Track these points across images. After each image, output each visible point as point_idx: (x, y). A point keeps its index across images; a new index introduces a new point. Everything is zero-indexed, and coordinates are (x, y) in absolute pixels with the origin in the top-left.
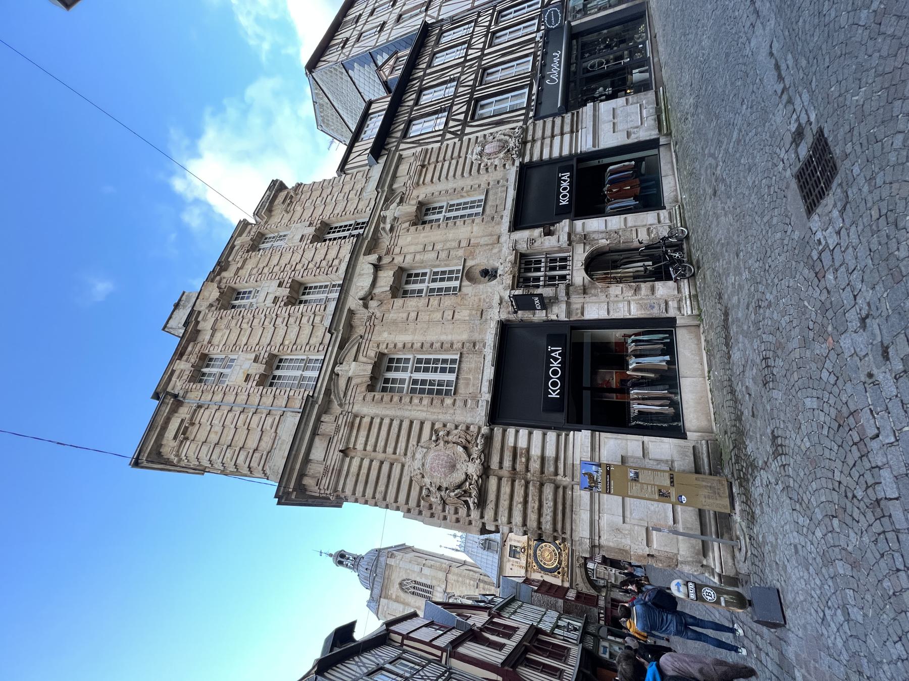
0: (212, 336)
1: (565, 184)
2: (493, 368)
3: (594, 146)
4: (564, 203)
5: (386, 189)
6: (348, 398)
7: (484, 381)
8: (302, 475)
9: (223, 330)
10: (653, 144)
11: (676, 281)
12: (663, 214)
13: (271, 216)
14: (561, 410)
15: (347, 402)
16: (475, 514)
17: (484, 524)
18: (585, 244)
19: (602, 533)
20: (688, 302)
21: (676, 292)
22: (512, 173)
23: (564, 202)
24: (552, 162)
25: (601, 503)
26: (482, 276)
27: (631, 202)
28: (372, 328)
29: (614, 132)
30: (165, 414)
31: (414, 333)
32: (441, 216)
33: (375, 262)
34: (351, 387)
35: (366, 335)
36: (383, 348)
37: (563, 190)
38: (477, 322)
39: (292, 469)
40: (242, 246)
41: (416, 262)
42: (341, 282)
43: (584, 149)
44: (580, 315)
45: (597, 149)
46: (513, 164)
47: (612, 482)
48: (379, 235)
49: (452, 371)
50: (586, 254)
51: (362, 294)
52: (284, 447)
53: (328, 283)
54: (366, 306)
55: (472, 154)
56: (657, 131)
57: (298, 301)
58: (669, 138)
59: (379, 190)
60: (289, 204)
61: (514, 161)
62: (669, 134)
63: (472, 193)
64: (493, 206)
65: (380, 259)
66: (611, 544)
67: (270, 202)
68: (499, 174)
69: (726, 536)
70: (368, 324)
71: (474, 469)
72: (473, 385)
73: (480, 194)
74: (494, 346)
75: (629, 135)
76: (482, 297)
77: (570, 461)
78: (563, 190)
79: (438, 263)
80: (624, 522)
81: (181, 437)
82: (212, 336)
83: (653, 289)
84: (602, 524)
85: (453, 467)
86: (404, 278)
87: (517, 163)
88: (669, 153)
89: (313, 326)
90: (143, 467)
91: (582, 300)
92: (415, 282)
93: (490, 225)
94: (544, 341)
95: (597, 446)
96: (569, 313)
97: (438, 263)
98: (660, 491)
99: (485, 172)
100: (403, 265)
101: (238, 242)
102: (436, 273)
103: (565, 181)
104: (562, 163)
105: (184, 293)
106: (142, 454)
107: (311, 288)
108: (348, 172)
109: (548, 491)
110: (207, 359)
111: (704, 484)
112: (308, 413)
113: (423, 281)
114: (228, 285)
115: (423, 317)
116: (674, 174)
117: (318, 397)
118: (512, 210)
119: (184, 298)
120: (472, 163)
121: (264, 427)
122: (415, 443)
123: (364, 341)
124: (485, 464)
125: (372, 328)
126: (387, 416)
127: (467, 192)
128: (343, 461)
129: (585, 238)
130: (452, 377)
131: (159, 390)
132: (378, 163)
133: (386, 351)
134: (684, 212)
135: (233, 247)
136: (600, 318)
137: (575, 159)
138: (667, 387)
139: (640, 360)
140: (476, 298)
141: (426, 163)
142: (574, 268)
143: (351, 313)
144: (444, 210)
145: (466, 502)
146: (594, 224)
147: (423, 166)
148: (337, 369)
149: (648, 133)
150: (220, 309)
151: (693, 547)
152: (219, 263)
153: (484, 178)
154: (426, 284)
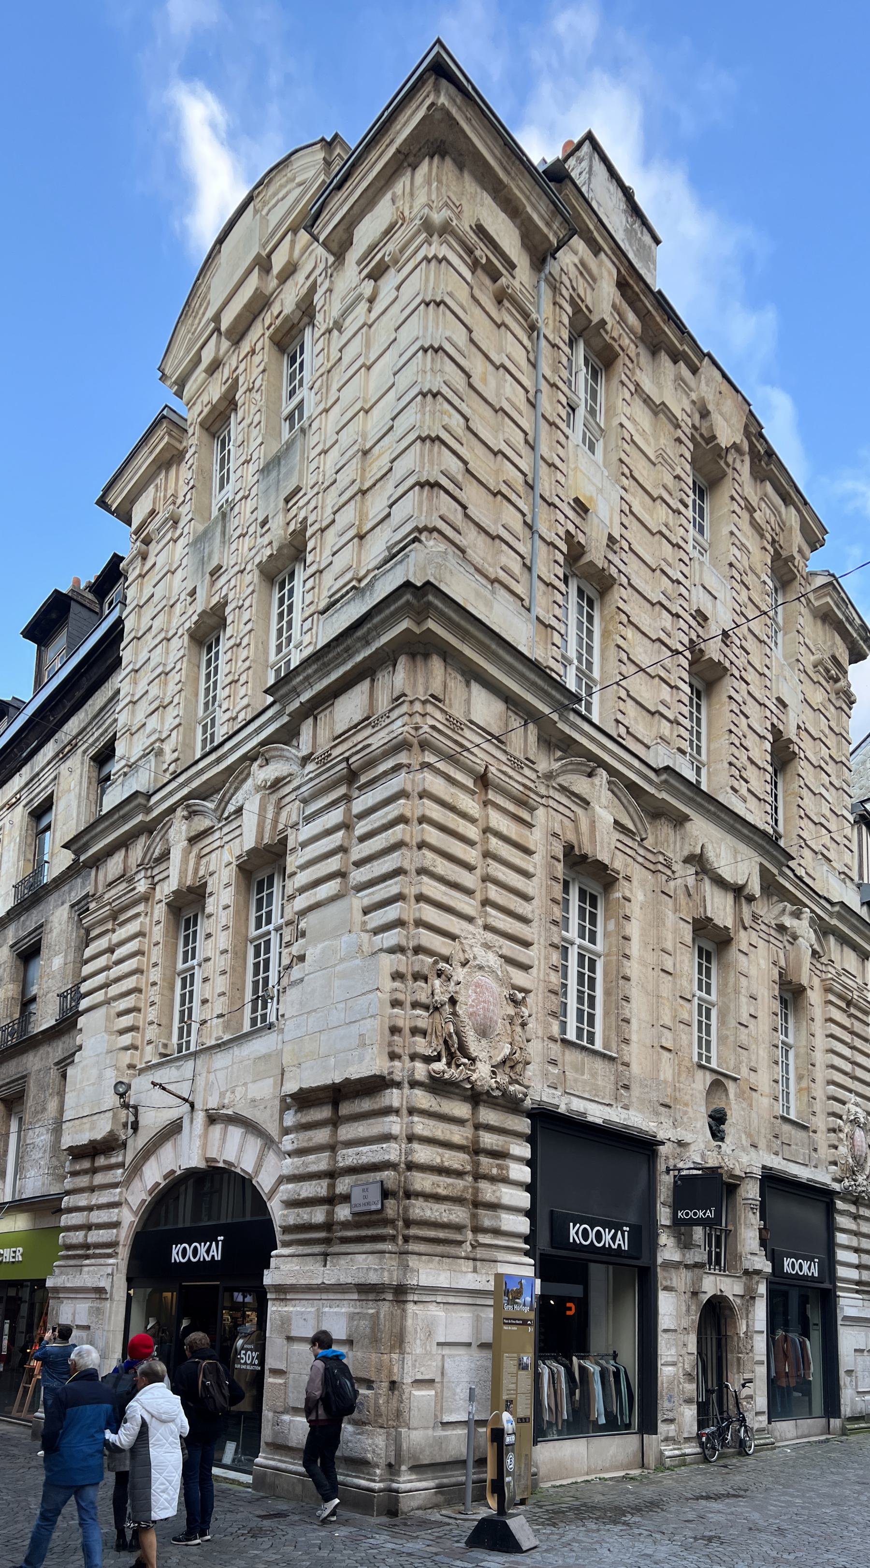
0: (647, 400)
1: (701, 1214)
2: (599, 1121)
3: (846, 1318)
4: (572, 1232)
5: (834, 922)
6: (557, 795)
7: (587, 1103)
8: (448, 654)
9: (657, 440)
10: (832, 1407)
11: (699, 1436)
12: (764, 1418)
13: (815, 617)
14: (553, 1243)
15: (552, 793)
16: (421, 1070)
17: (398, 1085)
18: (742, 1296)
19: (420, 1306)
20: (677, 1452)
21: (686, 1435)
22: (823, 1177)
23: (574, 1232)
24: (831, 1246)
25: (455, 1307)
26: (715, 1111)
27: (773, 1374)
28: (651, 867)
29: (856, 1350)
30: (529, 209)
31: (643, 963)
32: (573, 933)
33: (746, 891)
34: (574, 807)
35: (642, 851)
36: (622, 890)
37: (598, 1232)
38: (654, 1096)
39: (464, 635)
40: (782, 525)
41: (737, 980)
42: (704, 787)
43: (842, 1302)
44: (665, 1283)
45: (839, 1322)
46: (835, 1180)
47: (515, 1328)
48: (775, 898)
50: (731, 1298)
51: (710, 854)
52: (483, 609)
53: (704, 757)
54: (690, 859)
55: (857, 1105)
56: (849, 1414)
58: (839, 1432)
59: (837, 908)
60: (827, 671)
61: (840, 1181)
62: (844, 1432)
63: (806, 1099)
64: (790, 1139)
65: (751, 899)
66: (409, 1322)
67: (841, 621)
68: (825, 1153)
69: (440, 1499)
70: (661, 859)
71: (482, 1074)
72: (576, 1080)
73: (798, 1112)
74: (627, 1127)
75: (849, 1372)
76: (690, 1110)
77: (501, 1256)
78: (598, 1232)
79: (733, 1023)
80: (439, 1344)
81: (482, 252)
82: (647, 400)
83: (689, 1401)
84: (432, 1307)
85: (483, 1032)
87: (836, 1187)
88: (819, 1432)
89: (653, 714)
90: (421, 81)
91: (681, 1287)
93: (768, 1131)
94: (633, 1219)
95: (479, 1301)
96: (669, 1265)
97: (733, 1023)
98: (511, 1402)
99: (831, 1126)
100: (733, 951)
101: (792, 517)
103: (614, 1239)
104: (829, 1264)
105: (657, 242)
106: (459, 99)
108: (856, 830)
109: (458, 1214)
111: (523, 1466)
112: (701, 806)
114: (729, 471)
115: (666, 984)
116: (797, 1438)
117: (567, 721)
118: (785, 1172)
119: (647, 239)
120: (844, 1103)
121: (505, 547)
122: (504, 951)
123: (636, 846)
124: (485, 1097)
125: (651, 867)
126: (824, 1012)
127: (808, 1089)
128: (468, 770)
129: (750, 1297)
130: (571, 1035)
131: (569, 189)
132: (863, 904)
133: (618, 895)
134: (768, 1449)
135: (786, 499)
136: (660, 1317)
137: (830, 1286)
138: (571, 1419)
139: (597, 1378)
140: (688, 1097)
141: (853, 1010)
142: (718, 1278)
143: (680, 821)
144: (586, 943)
145: (438, 1058)
146: (760, 1312)
147: (849, 1003)
148: (603, 774)
149: (848, 1402)
150: (693, 439)
151: (422, 1451)
152: (770, 453)
153: (821, 1123)
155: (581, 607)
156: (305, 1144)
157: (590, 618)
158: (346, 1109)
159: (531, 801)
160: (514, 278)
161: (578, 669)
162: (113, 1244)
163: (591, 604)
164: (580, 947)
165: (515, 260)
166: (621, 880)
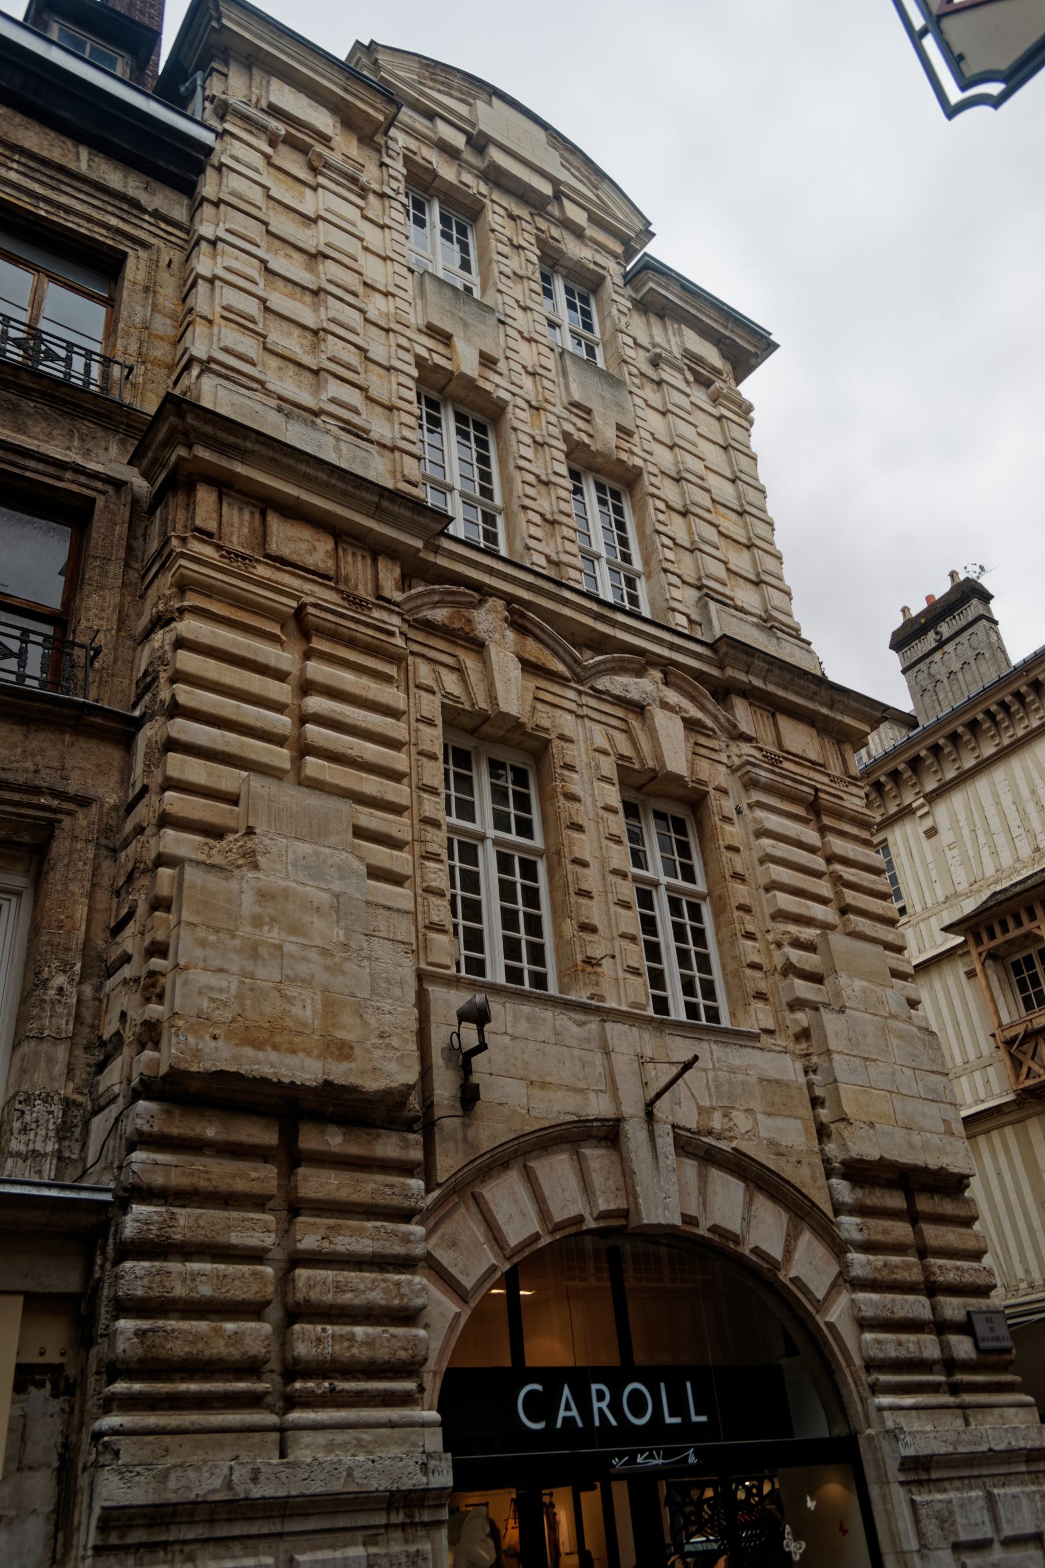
32: (484, 822)
49: (692, 1010)
53: (498, 500)
57: (434, 395)
86: (511, 758)
92: (499, 794)
102: (529, 870)
107: (482, 444)
110: (465, 221)
113: (501, 822)
130: (678, 1012)
141: (826, 820)
144: (680, 882)
154: (492, 833)
155: (602, 502)
156: (879, 1237)
157: (619, 511)
158: (310, 1140)
159: (341, 629)
160: (332, 149)
161: (608, 562)
162: (410, 1368)
163: (616, 496)
164: (496, 842)
165: (329, 131)
166: (712, 792)
